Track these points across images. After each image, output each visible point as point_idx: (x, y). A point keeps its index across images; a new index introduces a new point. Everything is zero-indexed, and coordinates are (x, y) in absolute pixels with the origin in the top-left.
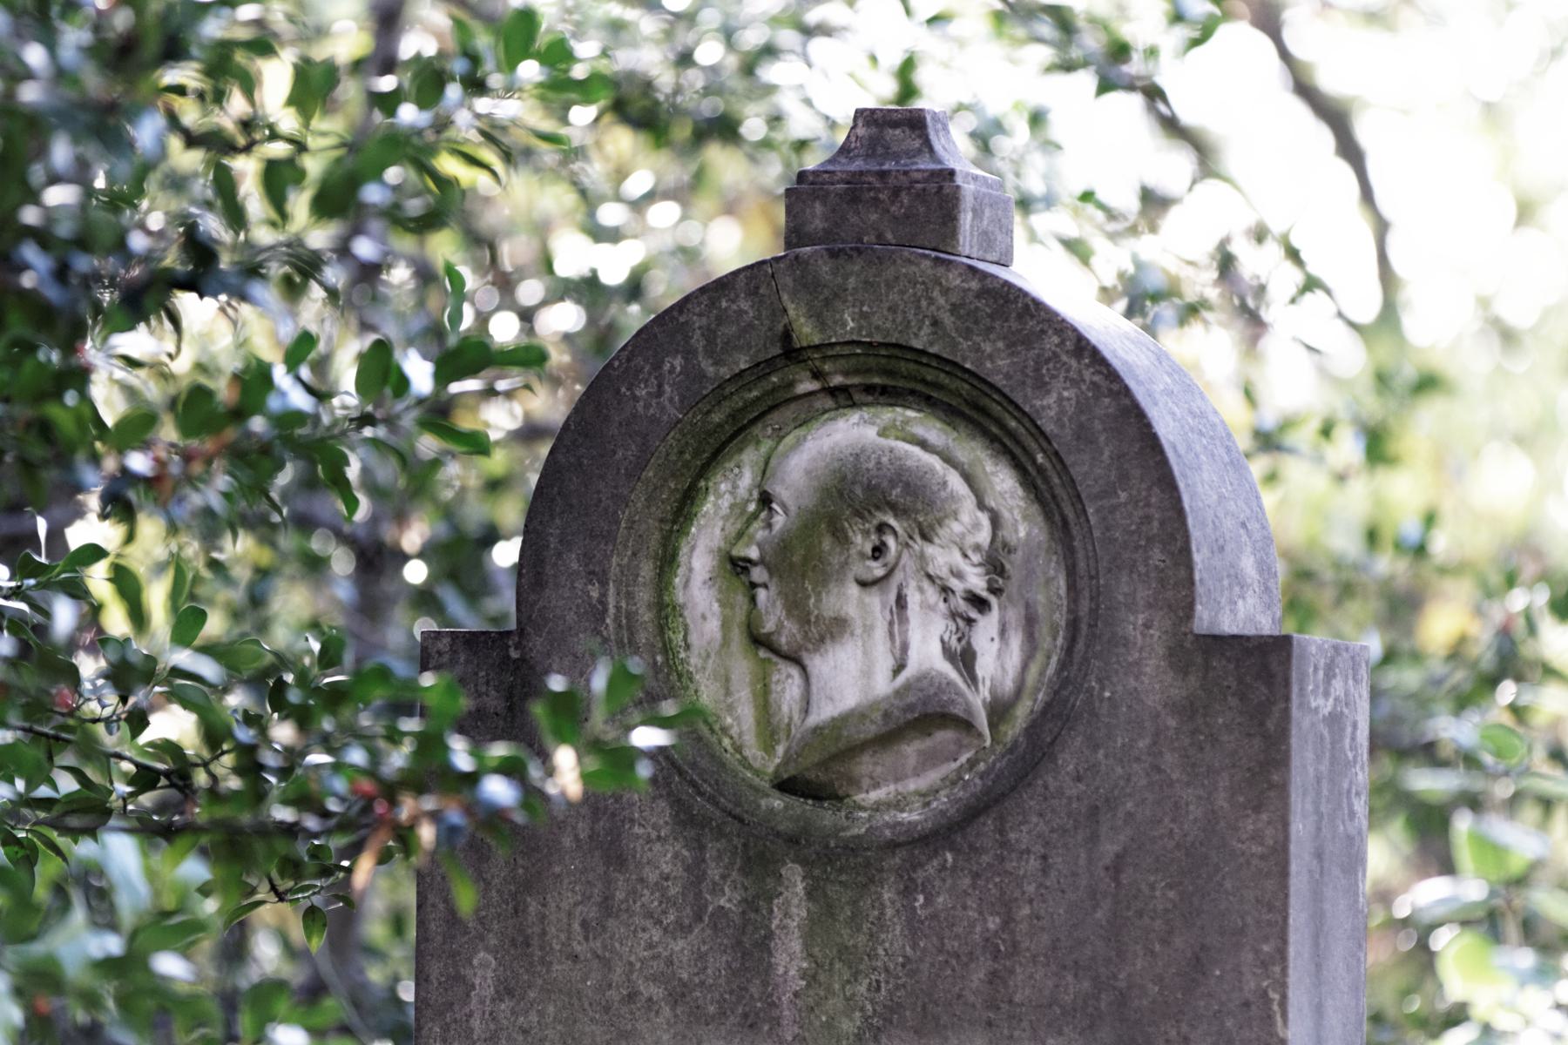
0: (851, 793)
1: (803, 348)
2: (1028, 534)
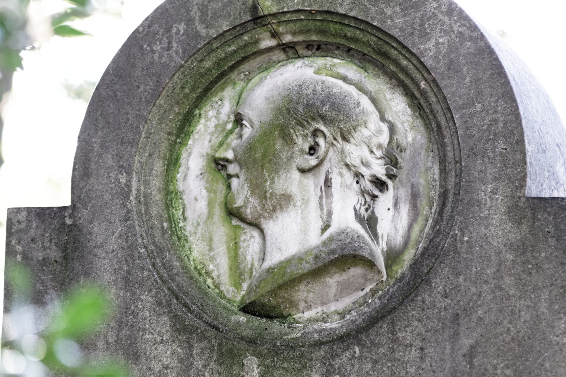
0: (292, 313)
1: (265, 16)
2: (414, 139)
